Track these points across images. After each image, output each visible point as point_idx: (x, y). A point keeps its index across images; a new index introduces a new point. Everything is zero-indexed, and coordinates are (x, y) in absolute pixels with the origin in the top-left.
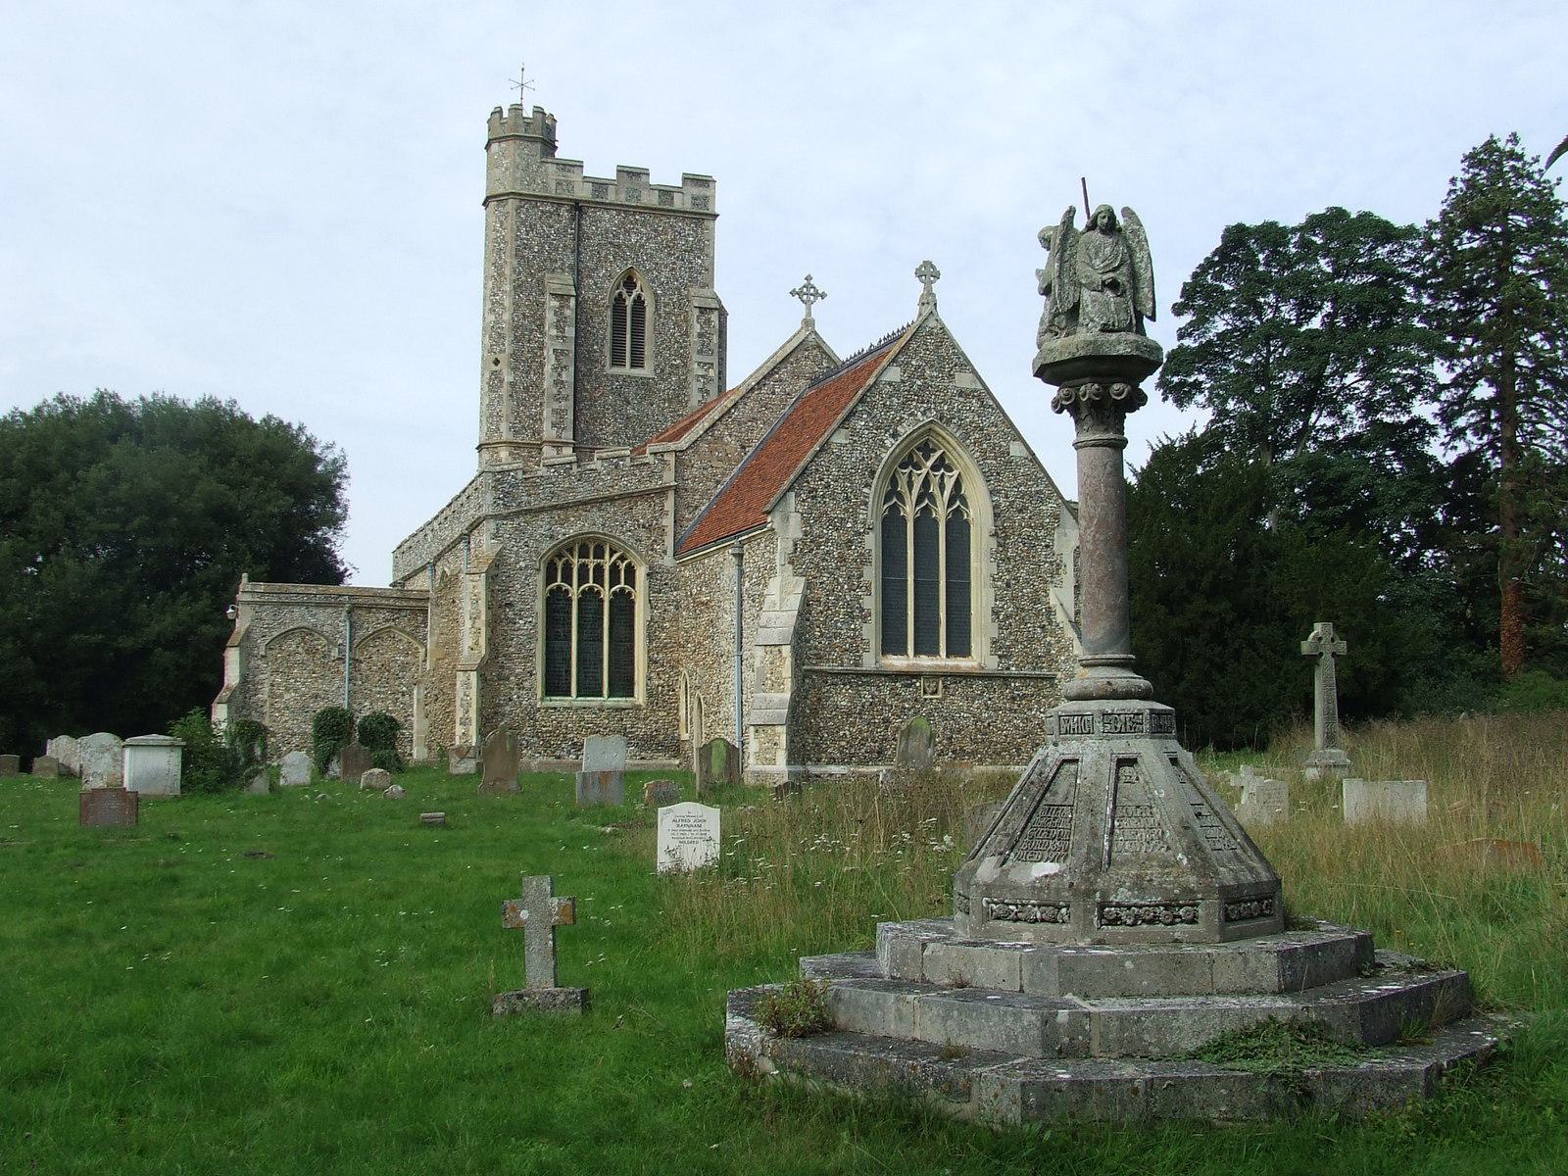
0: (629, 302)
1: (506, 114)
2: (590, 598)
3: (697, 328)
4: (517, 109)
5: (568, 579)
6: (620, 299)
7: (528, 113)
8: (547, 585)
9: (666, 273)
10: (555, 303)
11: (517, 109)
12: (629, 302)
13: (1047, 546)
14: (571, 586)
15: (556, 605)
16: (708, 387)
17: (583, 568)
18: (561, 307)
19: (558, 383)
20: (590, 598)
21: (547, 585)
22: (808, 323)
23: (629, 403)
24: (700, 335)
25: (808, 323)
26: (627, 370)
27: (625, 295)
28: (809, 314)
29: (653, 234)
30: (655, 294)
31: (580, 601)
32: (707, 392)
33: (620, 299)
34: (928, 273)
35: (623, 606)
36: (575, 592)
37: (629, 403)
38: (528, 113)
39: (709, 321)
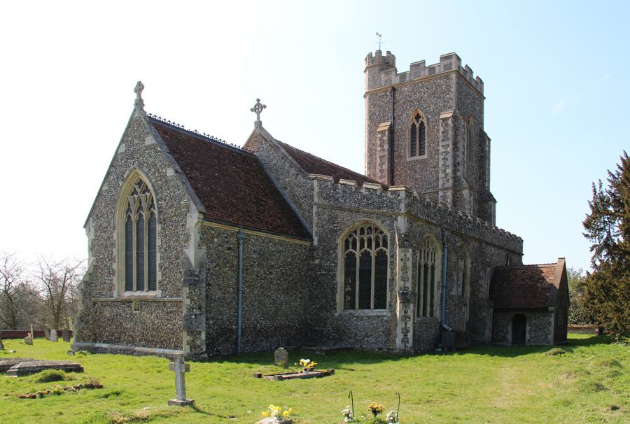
0: (418, 126)
1: (374, 55)
2: (366, 256)
3: (441, 129)
4: (379, 52)
5: (354, 247)
6: (414, 126)
7: (384, 54)
8: (345, 251)
9: (433, 107)
10: (380, 136)
11: (379, 52)
12: (418, 126)
13: (183, 225)
14: (356, 250)
15: (350, 259)
16: (447, 157)
17: (362, 241)
18: (382, 137)
19: (382, 171)
20: (366, 256)
21: (345, 251)
22: (259, 124)
23: (416, 172)
24: (443, 132)
25: (259, 124)
26: (417, 157)
27: (416, 123)
28: (258, 118)
29: (427, 90)
30: (428, 118)
31: (376, 257)
32: (447, 159)
33: (414, 126)
34: (139, 88)
35: (382, 257)
36: (358, 254)
37: (416, 172)
38: (384, 54)
39: (447, 124)
